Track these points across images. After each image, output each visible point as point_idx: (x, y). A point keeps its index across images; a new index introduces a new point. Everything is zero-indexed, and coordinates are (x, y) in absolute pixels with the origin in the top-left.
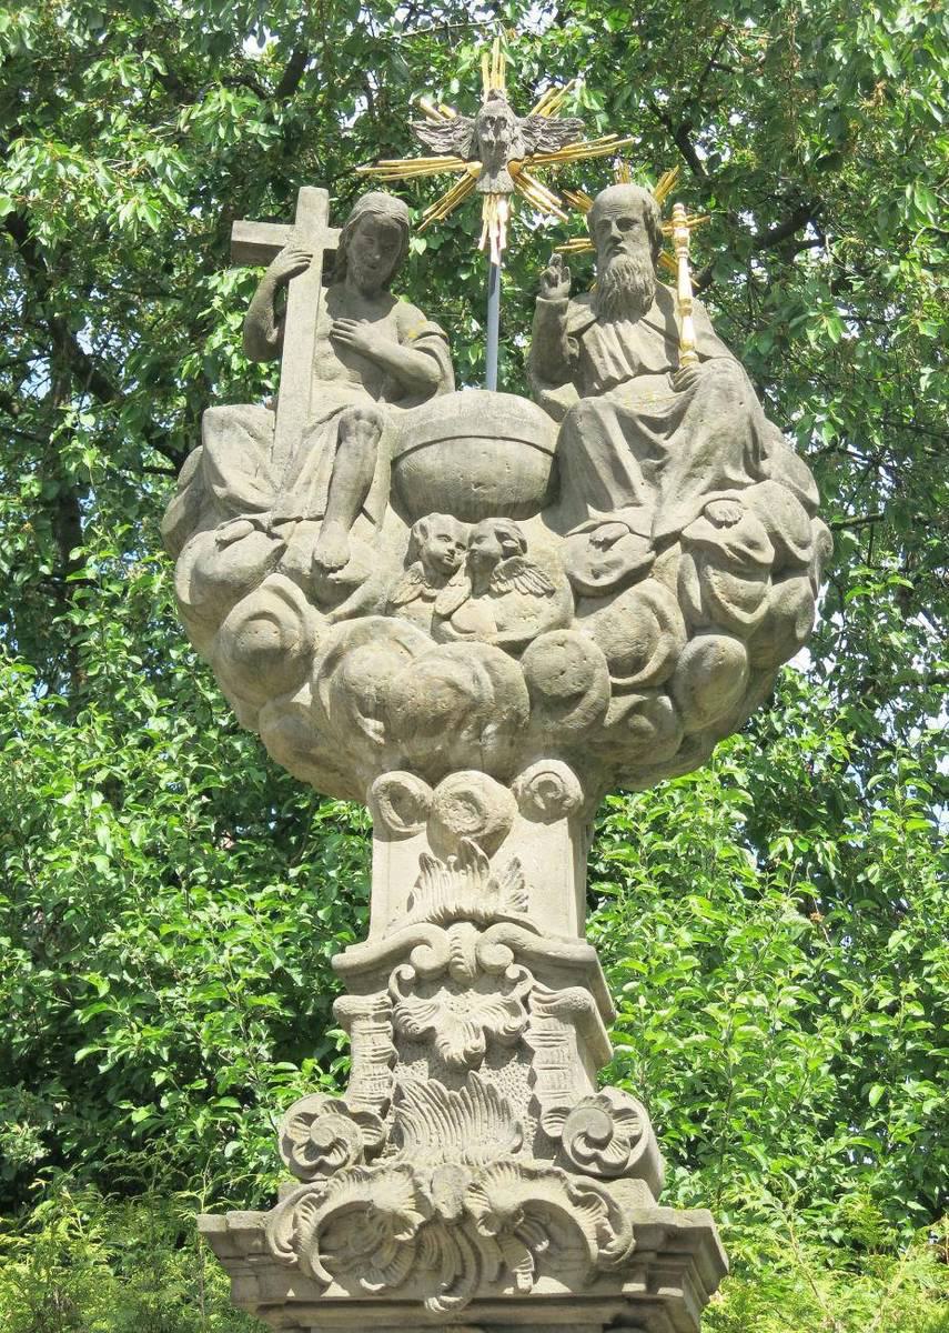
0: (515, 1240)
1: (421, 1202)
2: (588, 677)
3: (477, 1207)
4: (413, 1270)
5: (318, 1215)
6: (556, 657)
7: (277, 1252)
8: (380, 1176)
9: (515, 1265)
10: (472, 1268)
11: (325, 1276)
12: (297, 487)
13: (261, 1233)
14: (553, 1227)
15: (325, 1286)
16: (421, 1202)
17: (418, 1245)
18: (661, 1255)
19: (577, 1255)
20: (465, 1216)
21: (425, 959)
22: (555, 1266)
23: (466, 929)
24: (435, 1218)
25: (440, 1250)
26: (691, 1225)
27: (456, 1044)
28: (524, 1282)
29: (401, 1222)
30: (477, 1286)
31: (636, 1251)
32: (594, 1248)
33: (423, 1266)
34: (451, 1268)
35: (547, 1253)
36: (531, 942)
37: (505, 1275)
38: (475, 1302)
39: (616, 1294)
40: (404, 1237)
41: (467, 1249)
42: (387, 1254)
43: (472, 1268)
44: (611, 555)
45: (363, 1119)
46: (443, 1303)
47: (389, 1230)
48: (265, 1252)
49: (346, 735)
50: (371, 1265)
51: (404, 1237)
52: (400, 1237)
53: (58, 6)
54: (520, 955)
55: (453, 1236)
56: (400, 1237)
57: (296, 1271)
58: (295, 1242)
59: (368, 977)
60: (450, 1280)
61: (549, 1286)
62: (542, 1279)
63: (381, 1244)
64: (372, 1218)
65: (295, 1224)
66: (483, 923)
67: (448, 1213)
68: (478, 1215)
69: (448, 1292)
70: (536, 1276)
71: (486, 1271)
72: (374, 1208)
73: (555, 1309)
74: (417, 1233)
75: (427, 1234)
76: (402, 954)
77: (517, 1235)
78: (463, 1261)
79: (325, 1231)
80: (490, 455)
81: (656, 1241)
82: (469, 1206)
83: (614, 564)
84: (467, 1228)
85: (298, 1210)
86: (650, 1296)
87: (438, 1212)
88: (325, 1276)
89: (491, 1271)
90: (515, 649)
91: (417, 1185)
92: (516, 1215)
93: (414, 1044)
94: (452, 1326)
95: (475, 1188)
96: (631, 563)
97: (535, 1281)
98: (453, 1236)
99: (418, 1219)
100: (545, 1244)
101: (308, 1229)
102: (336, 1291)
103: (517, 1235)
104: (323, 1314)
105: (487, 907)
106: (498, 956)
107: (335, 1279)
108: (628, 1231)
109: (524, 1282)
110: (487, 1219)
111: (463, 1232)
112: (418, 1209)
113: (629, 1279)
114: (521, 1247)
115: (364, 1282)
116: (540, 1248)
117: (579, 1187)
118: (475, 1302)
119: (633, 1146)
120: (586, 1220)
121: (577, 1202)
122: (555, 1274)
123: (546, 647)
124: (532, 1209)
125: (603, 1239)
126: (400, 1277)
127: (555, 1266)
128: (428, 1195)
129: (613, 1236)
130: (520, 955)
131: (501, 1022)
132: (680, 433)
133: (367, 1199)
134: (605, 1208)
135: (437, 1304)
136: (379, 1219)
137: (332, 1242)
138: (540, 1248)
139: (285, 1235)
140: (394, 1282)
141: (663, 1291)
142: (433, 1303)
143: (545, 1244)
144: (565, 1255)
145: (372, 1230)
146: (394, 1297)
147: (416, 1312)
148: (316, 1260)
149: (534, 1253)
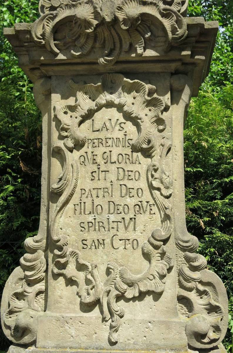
0: (137, 33)
1: (97, 15)
3: (121, 16)
4: (93, 48)
5: (52, 24)
7: (36, 39)
8: (79, 5)
9: (136, 44)
10: (118, 45)
11: (57, 51)
13: (29, 32)
14: (152, 27)
15: (57, 55)
16: (97, 15)
17: (95, 36)
18: (197, 42)
19: (163, 39)
20: (116, 20)
22: (153, 45)
24: (102, 22)
25: (105, 38)
26: (210, 27)
28: (140, 51)
29: (88, 24)
30: (120, 53)
31: (188, 37)
32: (170, 35)
33: (98, 45)
34: (109, 45)
35: (150, 39)
37: (132, 48)
38: (117, 62)
39: (178, 57)
40: (89, 31)
41: (73, 254)
42: (82, 40)
43: (118, 45)
46: (106, 60)
47: (83, 28)
48: (31, 40)
50: (76, 46)
51: (89, 31)
52: (88, 31)
53: (5, 199)
55: (110, 31)
56: (88, 31)
57: (43, 48)
58: (43, 35)
60: (109, 50)
61: (150, 53)
62: (147, 50)
63: (79, 36)
64: (76, 23)
65: (43, 28)
67: (108, 19)
68: (121, 20)
69: (108, 55)
70: (145, 49)
71: (124, 46)
72: (77, 18)
73: (152, 64)
74: (95, 29)
75: (99, 30)
77: (137, 30)
78: (114, 43)
79: (56, 30)
81: (196, 31)
82: (117, 15)
84: (116, 27)
85: (45, 22)
86: (192, 60)
87: (104, 18)
88: (57, 51)
89: (126, 47)
91: (95, 8)
92: (137, 19)
94: (109, 73)
95: (120, 9)
97: (144, 51)
98: (110, 31)
99: (95, 22)
100: (149, 34)
101: (48, 29)
102: (61, 57)
103: (137, 30)
104: (56, 68)
107: (60, 52)
108: (185, 27)
109: (140, 51)
110: (125, 21)
111: (114, 29)
112: (95, 18)
113: (184, 50)
114: (139, 35)
115: (72, 51)
116: (147, 36)
117: (164, 10)
119: (182, 5)
120: (167, 23)
121: (163, 15)
122: (153, 48)
125: (174, 30)
126: (88, 50)
127: (153, 45)
128: (100, 11)
129: (178, 30)
133: (74, 14)
134: (175, 18)
135: (103, 60)
136: (78, 23)
137: (59, 36)
138: (147, 36)
139: (39, 33)
140: (85, 52)
141: (197, 57)
142: (102, 60)
143: (149, 34)
144: (157, 39)
145: (76, 29)
146: (85, 60)
147: (94, 67)
148: (52, 43)
149: (144, 38)
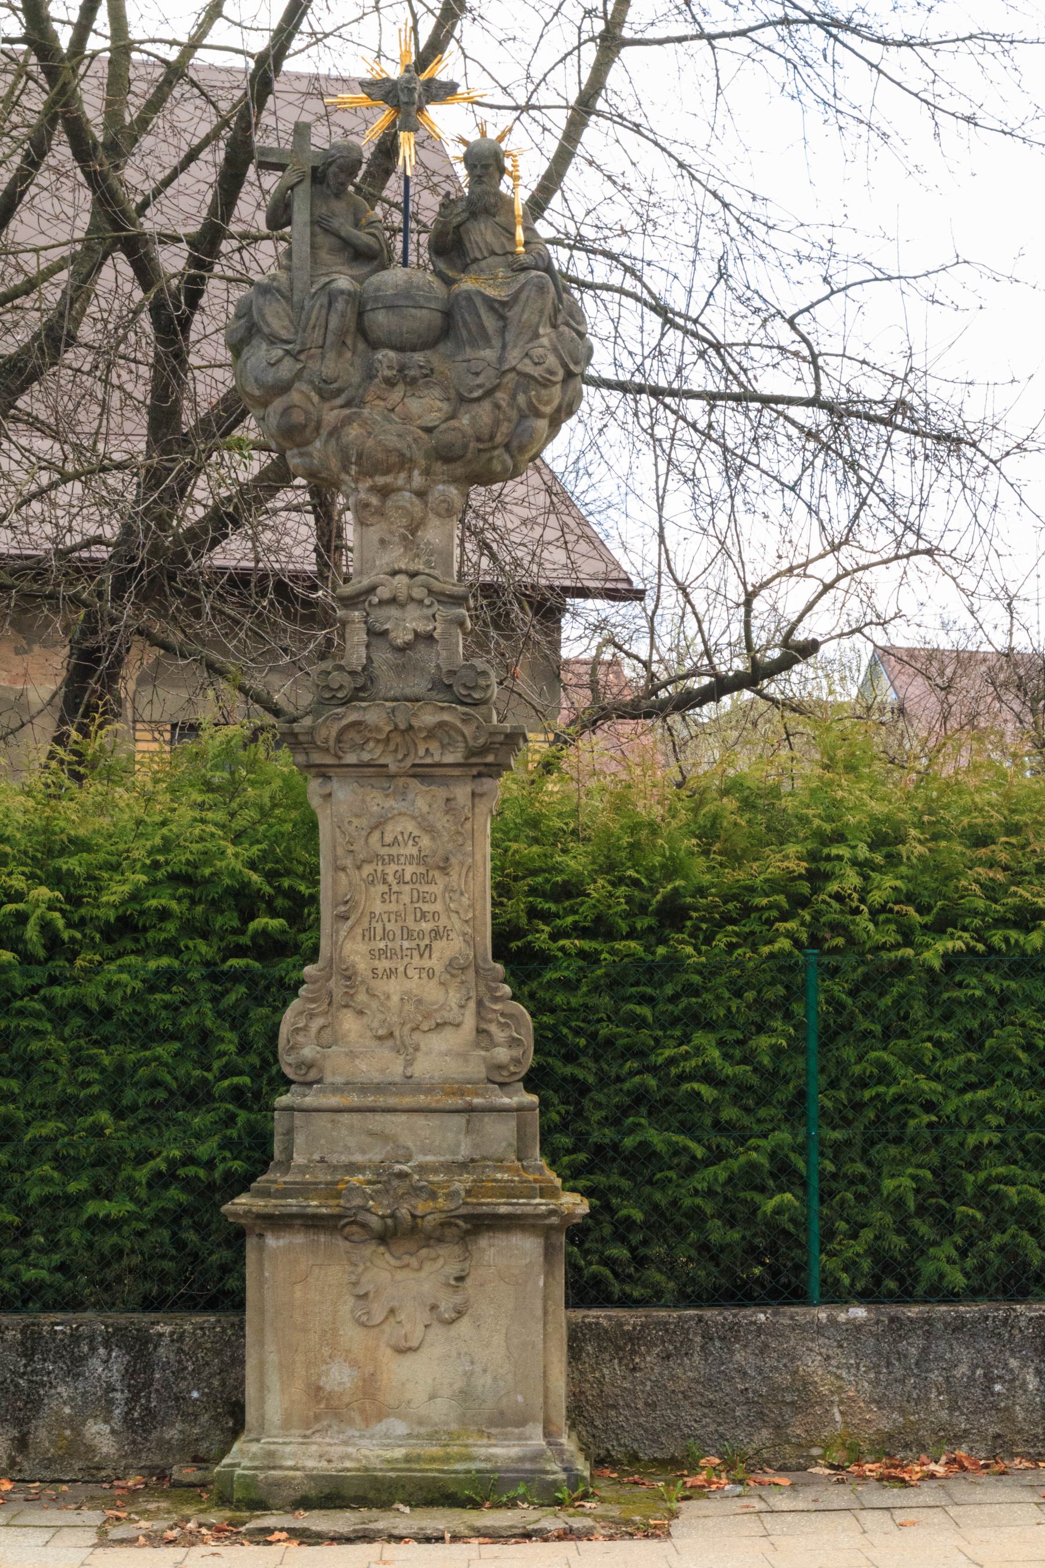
2: (465, 447)
6: (450, 437)
12: (309, 330)
21: (384, 593)
23: (403, 579)
27: (401, 637)
36: (437, 586)
44: (479, 380)
45: (353, 673)
49: (592, 39)
54: (431, 592)
59: (350, 602)
66: (413, 575)
76: (372, 589)
80: (413, 317)
83: (479, 386)
90: (429, 430)
93: (376, 634)
96: (488, 386)
99: (388, 729)
105: (413, 567)
106: (418, 593)
118: (414, 765)
123: (445, 431)
124: (441, 725)
130: (431, 592)
131: (422, 627)
132: (517, 309)
